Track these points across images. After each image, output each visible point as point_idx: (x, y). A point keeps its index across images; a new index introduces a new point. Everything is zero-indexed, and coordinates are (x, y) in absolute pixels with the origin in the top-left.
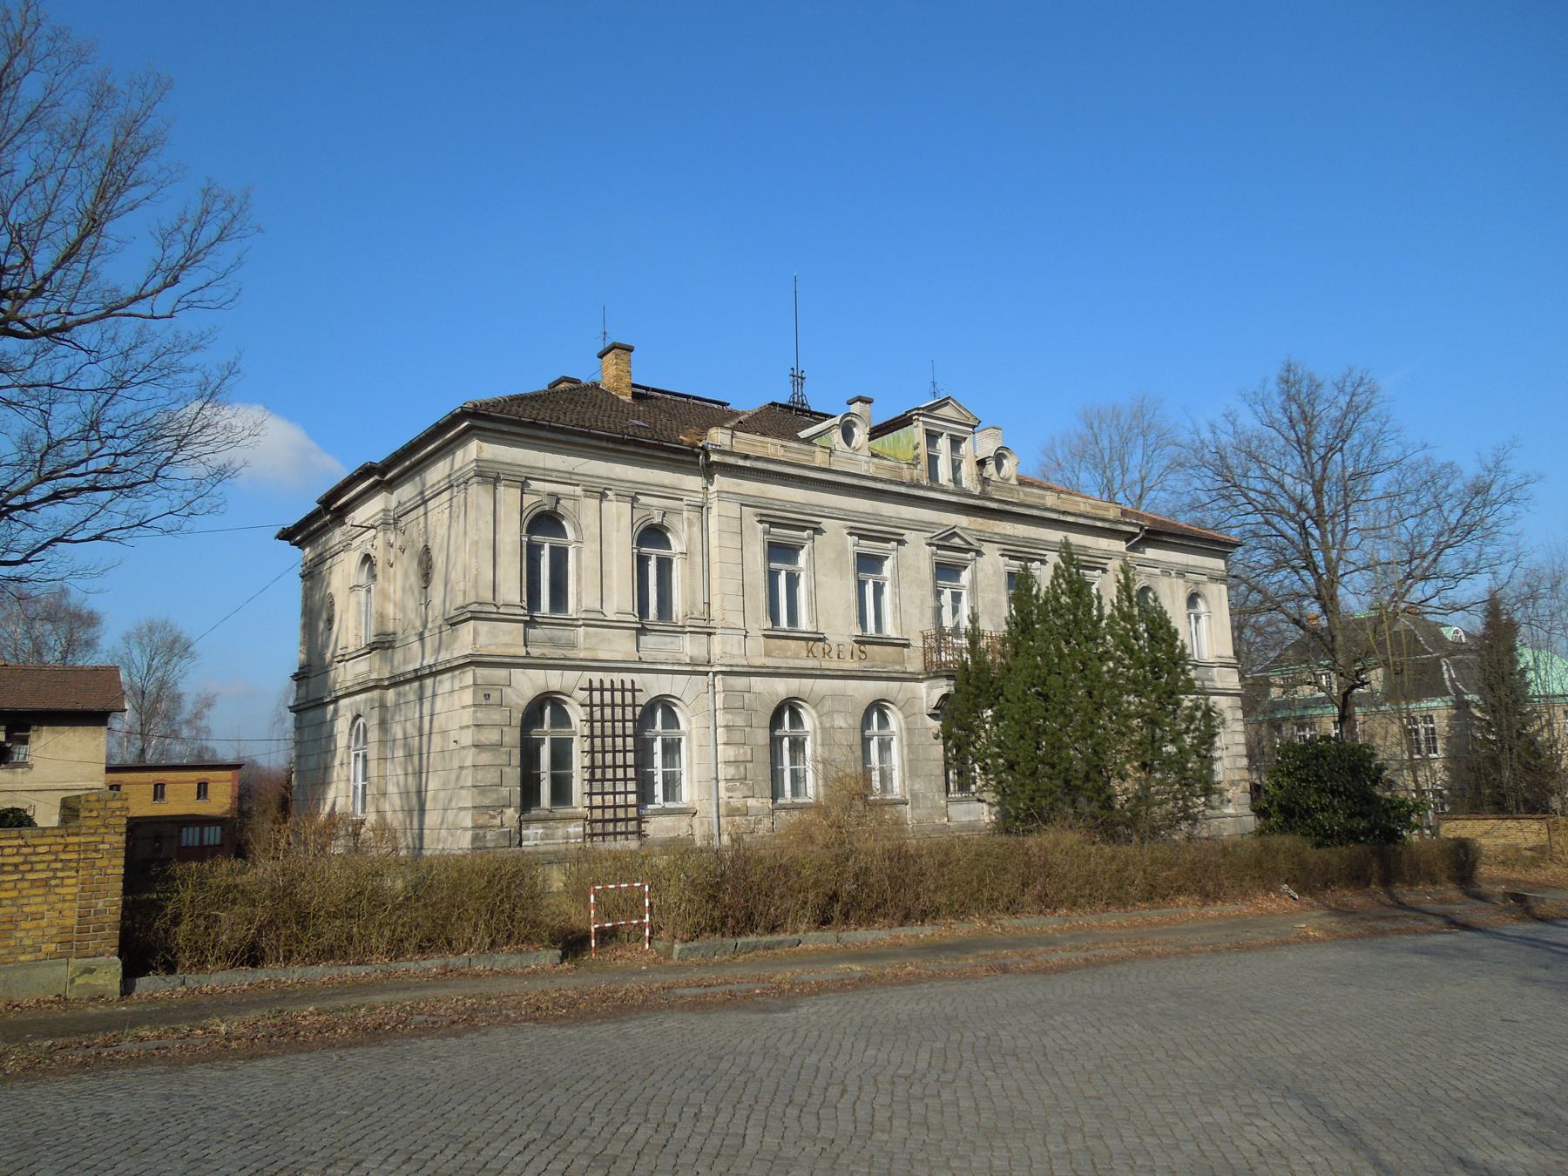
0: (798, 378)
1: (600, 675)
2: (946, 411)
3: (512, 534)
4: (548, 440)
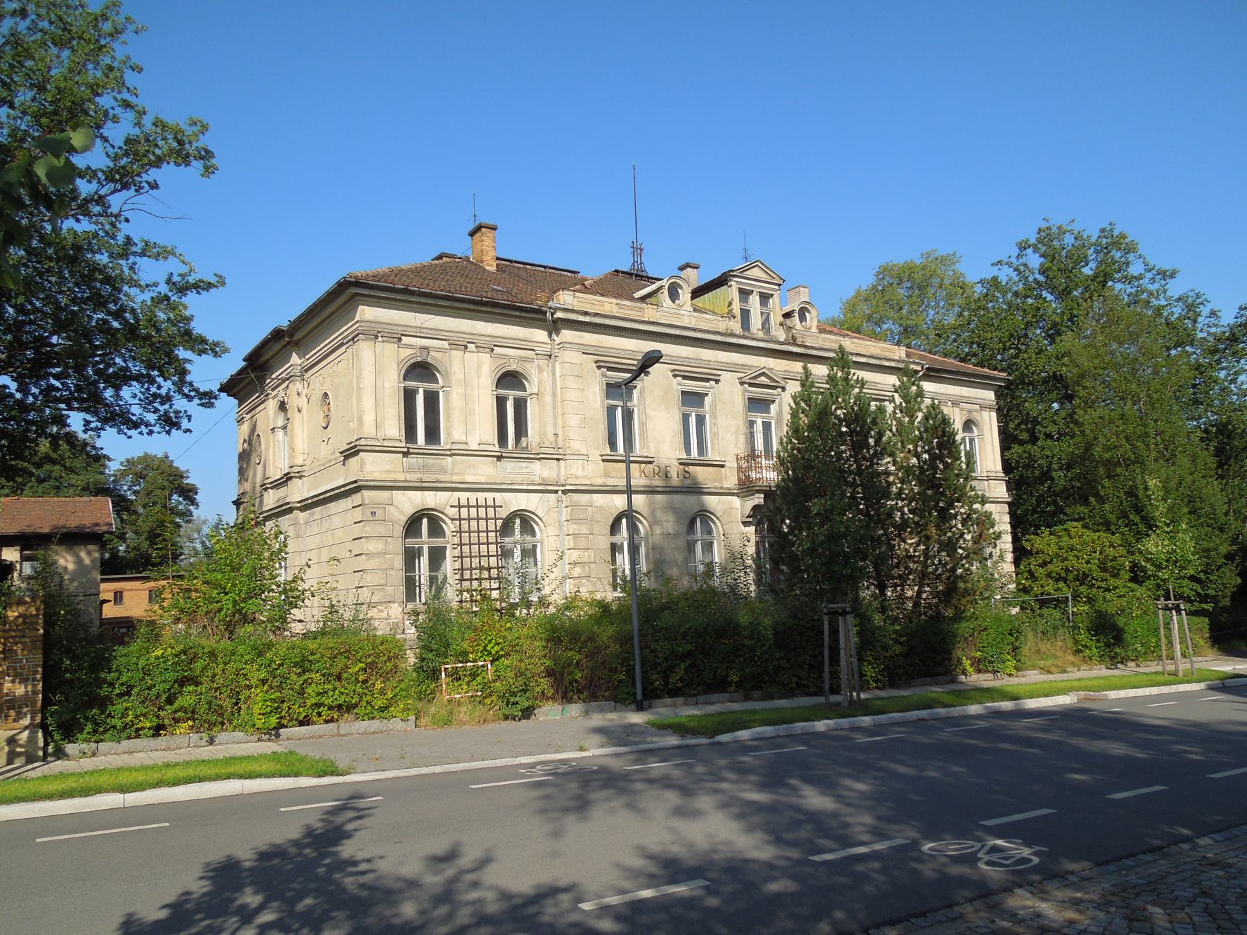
0: (637, 250)
1: (468, 494)
2: (756, 273)
3: (392, 383)
4: (419, 303)
